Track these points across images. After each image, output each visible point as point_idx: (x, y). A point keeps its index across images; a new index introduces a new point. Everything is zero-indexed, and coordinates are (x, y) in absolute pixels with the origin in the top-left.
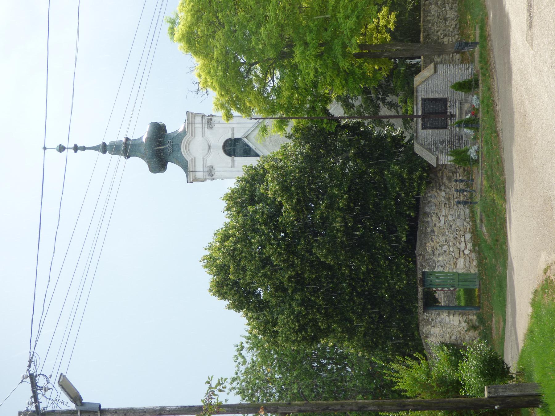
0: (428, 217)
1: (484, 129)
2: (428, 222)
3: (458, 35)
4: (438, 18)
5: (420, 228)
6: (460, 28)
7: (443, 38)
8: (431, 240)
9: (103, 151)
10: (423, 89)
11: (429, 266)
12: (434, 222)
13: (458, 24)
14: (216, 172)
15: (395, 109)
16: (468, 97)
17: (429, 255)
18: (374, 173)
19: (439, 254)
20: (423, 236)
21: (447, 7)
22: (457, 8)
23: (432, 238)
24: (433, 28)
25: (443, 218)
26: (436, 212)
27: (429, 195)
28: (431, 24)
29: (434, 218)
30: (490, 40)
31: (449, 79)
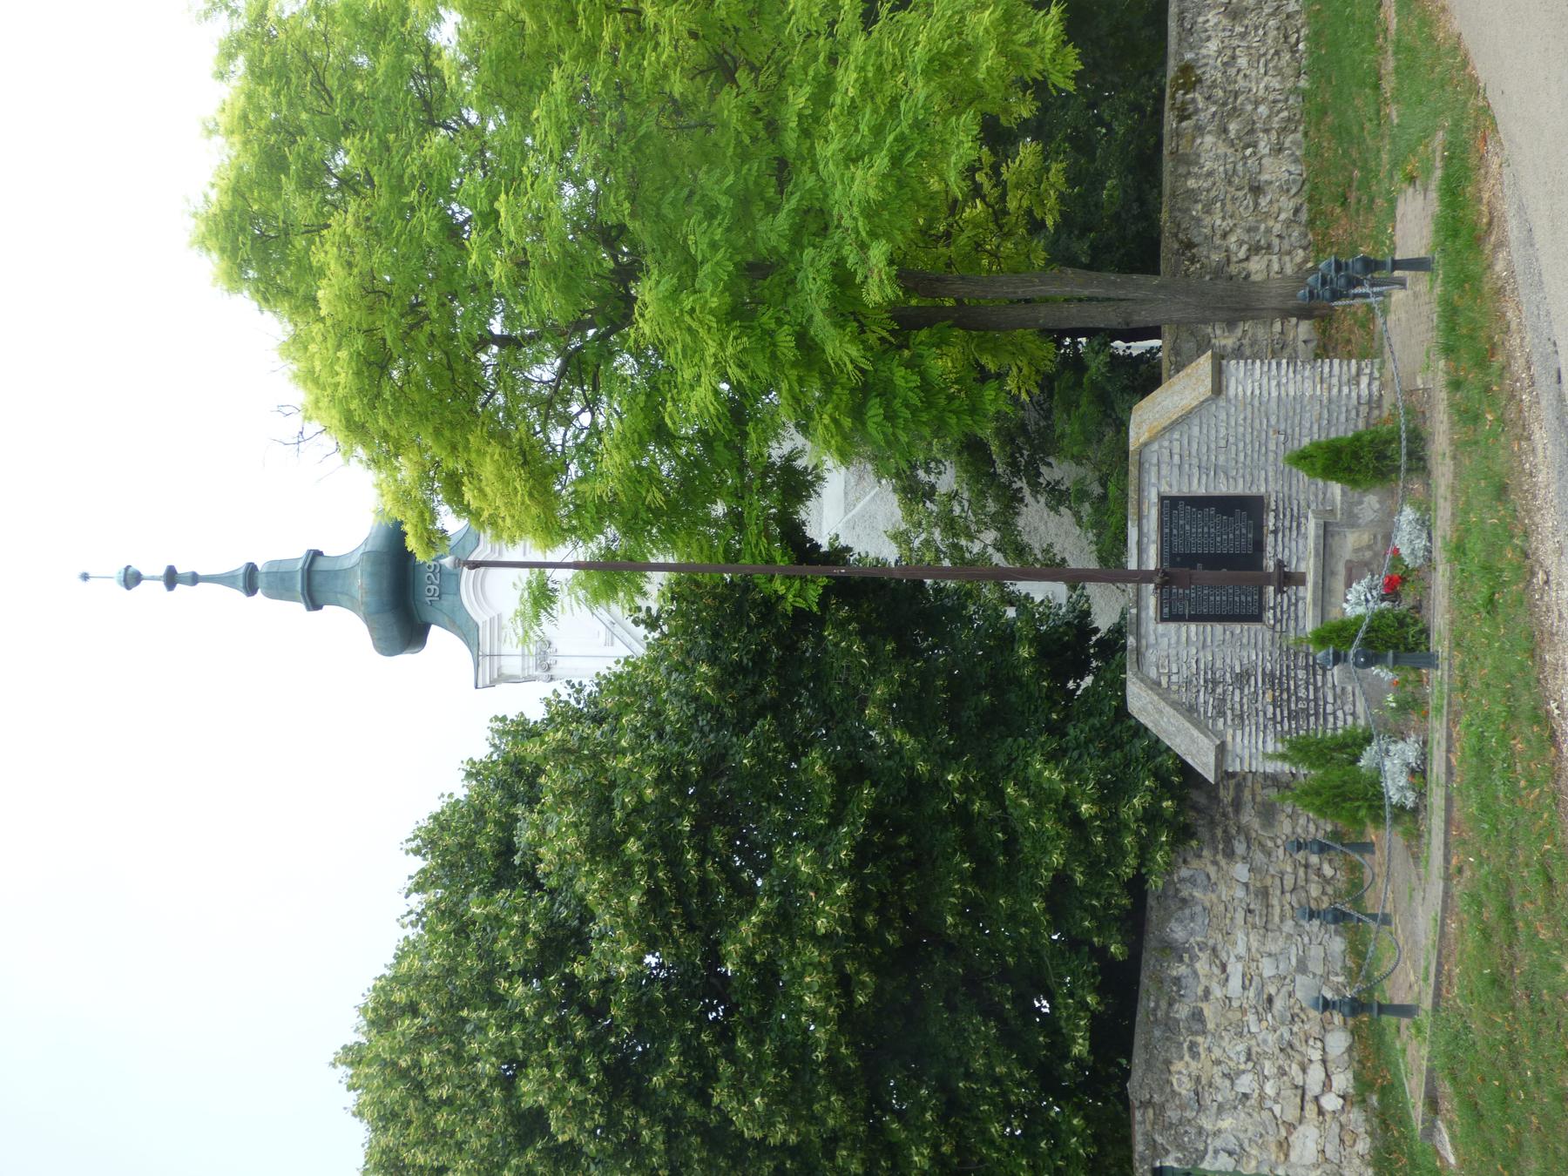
0: (1181, 960)
1: (1465, 685)
2: (1177, 981)
3: (1305, 249)
4: (1230, 183)
5: (1148, 1002)
6: (1311, 223)
7: (1247, 259)
8: (1190, 1049)
9: (245, 587)
10: (1166, 458)
11: (1180, 1147)
12: (1203, 979)
13: (1305, 206)
14: (559, 659)
15: (1070, 508)
16: (1361, 503)
17: (1183, 1107)
18: (965, 787)
19: (1220, 1108)
20: (1157, 1033)
21: (1262, 144)
22: (1299, 147)
23: (1193, 1045)
24: (1207, 220)
25: (1240, 966)
26: (1211, 942)
27: (1184, 872)
28: (1200, 206)
29: (1202, 966)
30: (1500, 244)
31: (1273, 420)
